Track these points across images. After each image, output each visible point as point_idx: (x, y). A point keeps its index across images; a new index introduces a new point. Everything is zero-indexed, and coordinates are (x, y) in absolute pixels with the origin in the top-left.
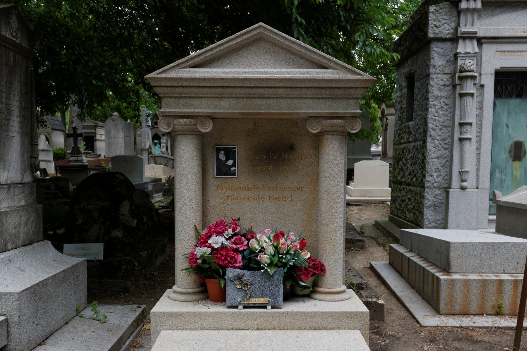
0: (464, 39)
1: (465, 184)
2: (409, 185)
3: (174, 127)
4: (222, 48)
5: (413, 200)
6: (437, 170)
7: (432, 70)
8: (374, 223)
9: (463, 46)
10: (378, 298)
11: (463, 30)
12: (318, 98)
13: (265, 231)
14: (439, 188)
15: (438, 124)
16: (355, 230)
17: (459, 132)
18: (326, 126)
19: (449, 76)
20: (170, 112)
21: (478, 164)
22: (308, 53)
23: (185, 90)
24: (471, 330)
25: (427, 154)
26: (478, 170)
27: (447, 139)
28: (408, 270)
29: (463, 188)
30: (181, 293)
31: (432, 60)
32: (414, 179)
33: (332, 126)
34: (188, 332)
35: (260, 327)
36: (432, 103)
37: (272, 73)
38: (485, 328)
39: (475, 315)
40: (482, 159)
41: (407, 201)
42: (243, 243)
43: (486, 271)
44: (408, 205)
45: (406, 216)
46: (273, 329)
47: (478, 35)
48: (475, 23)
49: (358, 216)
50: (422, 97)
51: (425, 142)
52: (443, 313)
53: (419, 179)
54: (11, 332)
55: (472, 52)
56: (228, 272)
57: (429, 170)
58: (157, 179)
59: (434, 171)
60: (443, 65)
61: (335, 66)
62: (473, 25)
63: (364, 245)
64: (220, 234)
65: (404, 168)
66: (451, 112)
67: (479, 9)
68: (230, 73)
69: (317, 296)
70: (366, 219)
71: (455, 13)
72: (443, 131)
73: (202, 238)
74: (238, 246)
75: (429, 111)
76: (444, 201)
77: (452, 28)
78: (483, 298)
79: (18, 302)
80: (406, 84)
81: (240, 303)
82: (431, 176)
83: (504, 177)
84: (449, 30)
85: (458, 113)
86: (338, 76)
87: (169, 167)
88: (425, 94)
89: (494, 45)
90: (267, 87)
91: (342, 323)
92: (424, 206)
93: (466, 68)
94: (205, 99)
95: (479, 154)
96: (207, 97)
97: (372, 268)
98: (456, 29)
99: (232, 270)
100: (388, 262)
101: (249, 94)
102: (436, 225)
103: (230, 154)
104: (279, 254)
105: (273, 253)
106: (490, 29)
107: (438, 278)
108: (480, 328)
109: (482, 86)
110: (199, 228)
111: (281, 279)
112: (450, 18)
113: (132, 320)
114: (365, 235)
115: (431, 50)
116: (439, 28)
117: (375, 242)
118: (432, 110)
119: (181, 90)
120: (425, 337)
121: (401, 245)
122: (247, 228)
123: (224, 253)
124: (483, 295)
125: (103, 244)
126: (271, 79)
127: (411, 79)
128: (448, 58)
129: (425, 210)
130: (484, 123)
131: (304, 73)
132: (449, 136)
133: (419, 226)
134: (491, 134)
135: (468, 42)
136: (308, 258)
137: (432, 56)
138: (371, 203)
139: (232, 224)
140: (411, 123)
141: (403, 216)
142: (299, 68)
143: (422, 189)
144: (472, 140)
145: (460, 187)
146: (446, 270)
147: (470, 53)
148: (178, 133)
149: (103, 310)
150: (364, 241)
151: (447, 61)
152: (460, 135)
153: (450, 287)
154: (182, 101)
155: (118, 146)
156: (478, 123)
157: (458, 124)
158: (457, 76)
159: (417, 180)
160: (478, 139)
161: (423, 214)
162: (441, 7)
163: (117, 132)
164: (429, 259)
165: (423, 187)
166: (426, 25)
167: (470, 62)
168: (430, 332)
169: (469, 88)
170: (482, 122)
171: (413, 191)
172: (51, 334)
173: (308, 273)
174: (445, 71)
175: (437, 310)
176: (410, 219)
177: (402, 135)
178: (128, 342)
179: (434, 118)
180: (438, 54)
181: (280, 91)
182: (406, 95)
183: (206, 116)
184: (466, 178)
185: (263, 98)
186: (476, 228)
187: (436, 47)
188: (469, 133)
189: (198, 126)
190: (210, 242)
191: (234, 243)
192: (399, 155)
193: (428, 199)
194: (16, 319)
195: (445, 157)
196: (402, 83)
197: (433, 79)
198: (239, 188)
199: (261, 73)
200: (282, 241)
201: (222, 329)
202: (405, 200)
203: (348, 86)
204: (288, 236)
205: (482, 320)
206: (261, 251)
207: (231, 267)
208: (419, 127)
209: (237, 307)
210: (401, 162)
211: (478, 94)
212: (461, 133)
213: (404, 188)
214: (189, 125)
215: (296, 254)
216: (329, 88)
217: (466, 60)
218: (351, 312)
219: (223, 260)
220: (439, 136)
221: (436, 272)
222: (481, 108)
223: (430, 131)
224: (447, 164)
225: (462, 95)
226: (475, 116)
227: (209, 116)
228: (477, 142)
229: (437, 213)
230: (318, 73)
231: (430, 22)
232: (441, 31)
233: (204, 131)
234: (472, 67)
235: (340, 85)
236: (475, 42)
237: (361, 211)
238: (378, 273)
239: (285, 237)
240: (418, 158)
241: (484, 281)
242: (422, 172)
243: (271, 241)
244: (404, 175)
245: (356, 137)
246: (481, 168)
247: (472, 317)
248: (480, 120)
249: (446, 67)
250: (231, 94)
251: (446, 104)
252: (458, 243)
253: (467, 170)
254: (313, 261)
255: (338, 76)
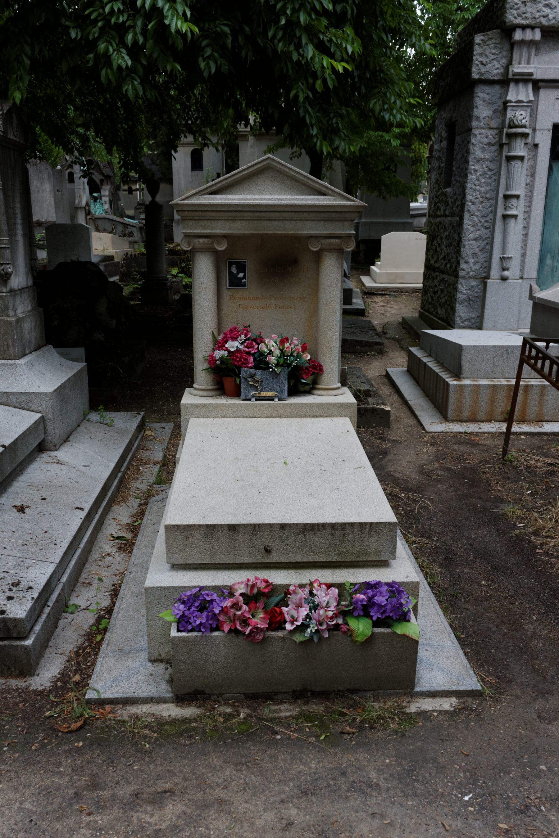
0: (517, 81)
1: (506, 273)
2: (442, 272)
3: (193, 246)
4: (235, 177)
5: (445, 292)
6: (475, 255)
7: (474, 123)
8: (401, 320)
9: (514, 91)
10: (385, 405)
11: (516, 70)
12: (318, 220)
13: (272, 336)
14: (475, 278)
15: (479, 196)
16: (375, 330)
17: (504, 207)
18: (324, 244)
19: (496, 131)
20: (191, 233)
21: (524, 247)
22: (310, 182)
23: (203, 214)
24: (475, 435)
25: (463, 234)
26: (524, 255)
27: (488, 215)
28: (424, 377)
29: (504, 279)
30: (202, 390)
31: (475, 110)
32: (448, 266)
33: (330, 244)
34: (211, 419)
35: (269, 416)
36: (473, 167)
37: (279, 200)
38: (489, 433)
39: (483, 421)
40: (529, 241)
41: (439, 292)
42: (254, 347)
43: (498, 376)
44: (441, 298)
45: (437, 313)
46: (279, 417)
47: (534, 77)
48: (532, 60)
49: (380, 310)
50: (462, 158)
51: (462, 218)
52: (451, 419)
53: (454, 265)
54: (47, 427)
55: (525, 101)
56: (242, 372)
57: (464, 255)
58: (108, 256)
59: (471, 256)
60: (488, 117)
61: (332, 194)
62: (528, 63)
63: (383, 348)
64: (234, 339)
65: (439, 249)
66: (495, 180)
67: (537, 41)
68: (243, 199)
69: (316, 392)
70: (393, 314)
71: (507, 46)
72: (484, 204)
73: (220, 343)
74: (250, 349)
75: (469, 178)
76: (481, 294)
77: (503, 67)
78: (493, 403)
79: (52, 401)
80: (446, 134)
81: (253, 396)
82: (467, 262)
83: (556, 264)
84: (498, 68)
85: (503, 181)
86: (335, 202)
87: (117, 236)
88: (465, 155)
89: (554, 90)
90: (274, 211)
91: (335, 412)
92: (456, 301)
93: (516, 123)
94: (221, 221)
95: (526, 235)
96: (222, 220)
97: (388, 376)
98: (507, 68)
99: (246, 369)
100: (406, 369)
101: (259, 217)
102: (469, 324)
103: (242, 268)
104: (284, 356)
105: (279, 355)
106: (550, 68)
107: (448, 384)
108: (485, 433)
109: (536, 146)
110: (216, 334)
111: (286, 376)
112: (500, 53)
113: (136, 425)
114: (388, 336)
115: (475, 95)
116: (485, 65)
117: (398, 346)
118: (472, 177)
119: (200, 213)
120: (427, 442)
121: (421, 349)
122: (257, 334)
123: (239, 356)
124: (492, 401)
125: (83, 348)
126: (278, 205)
127: (451, 127)
128: (495, 107)
129: (457, 305)
130: (535, 194)
131: (306, 200)
132: (491, 212)
133: (449, 325)
134: (542, 208)
135: (521, 86)
136: (309, 360)
137: (475, 105)
138: (402, 292)
139: (244, 330)
140: (449, 190)
141: (434, 313)
142: (302, 195)
143: (456, 280)
144: (518, 218)
145: (500, 278)
146: (457, 375)
147: (523, 102)
148: (197, 250)
149: (110, 416)
150: (383, 344)
151: (494, 112)
152: (504, 210)
153: (459, 392)
154: (202, 223)
155: (45, 205)
156: (528, 194)
157: (502, 196)
158: (505, 132)
159: (451, 267)
160: (527, 216)
161: (455, 310)
162: (490, 37)
163: (41, 183)
164: (445, 364)
165: (457, 276)
166: (470, 60)
167: (521, 115)
168: (433, 437)
169: (519, 149)
170: (532, 193)
171: (447, 281)
172: (71, 434)
173: (309, 372)
174: (491, 125)
175: (445, 417)
176: (442, 316)
177: (439, 204)
178: (136, 445)
179: (474, 187)
180: (484, 102)
181: (286, 215)
182: (445, 150)
183: (221, 236)
184: (507, 266)
185: (271, 220)
186: (516, 327)
187: (481, 92)
188: (515, 208)
189: (215, 244)
190: (227, 346)
191: (246, 347)
192: (434, 231)
193: (461, 292)
194: (51, 416)
195: (485, 239)
196: (441, 132)
197: (476, 135)
198: (249, 298)
199: (270, 199)
200: (287, 345)
201: (239, 417)
202: (437, 292)
203: (343, 210)
204: (292, 341)
205: (489, 426)
206: (269, 354)
207: (245, 367)
208: (457, 198)
209: (250, 400)
210: (435, 242)
211: (530, 157)
212: (505, 209)
213: (437, 276)
214: (207, 244)
215: (299, 356)
216: (327, 212)
217: (517, 110)
218: (343, 403)
219: (238, 362)
220: (479, 211)
221: (447, 378)
222: (533, 175)
223: (468, 205)
224: (487, 247)
225: (510, 159)
226: (524, 185)
227: (224, 236)
228: (525, 219)
229: (472, 310)
230: (318, 200)
231: (474, 58)
232: (488, 70)
233: (220, 249)
234: (524, 121)
235: (337, 210)
236: (530, 87)
237: (387, 303)
238: (393, 380)
239: (290, 342)
240: (454, 238)
241: (495, 386)
242: (457, 257)
243: (277, 345)
244: (438, 258)
245: (387, 193)
246: (528, 253)
247: (479, 423)
248: (530, 191)
249: (492, 120)
250: (243, 217)
251: (489, 169)
252: (471, 346)
253: (510, 256)
254: (313, 362)
255: (335, 202)
